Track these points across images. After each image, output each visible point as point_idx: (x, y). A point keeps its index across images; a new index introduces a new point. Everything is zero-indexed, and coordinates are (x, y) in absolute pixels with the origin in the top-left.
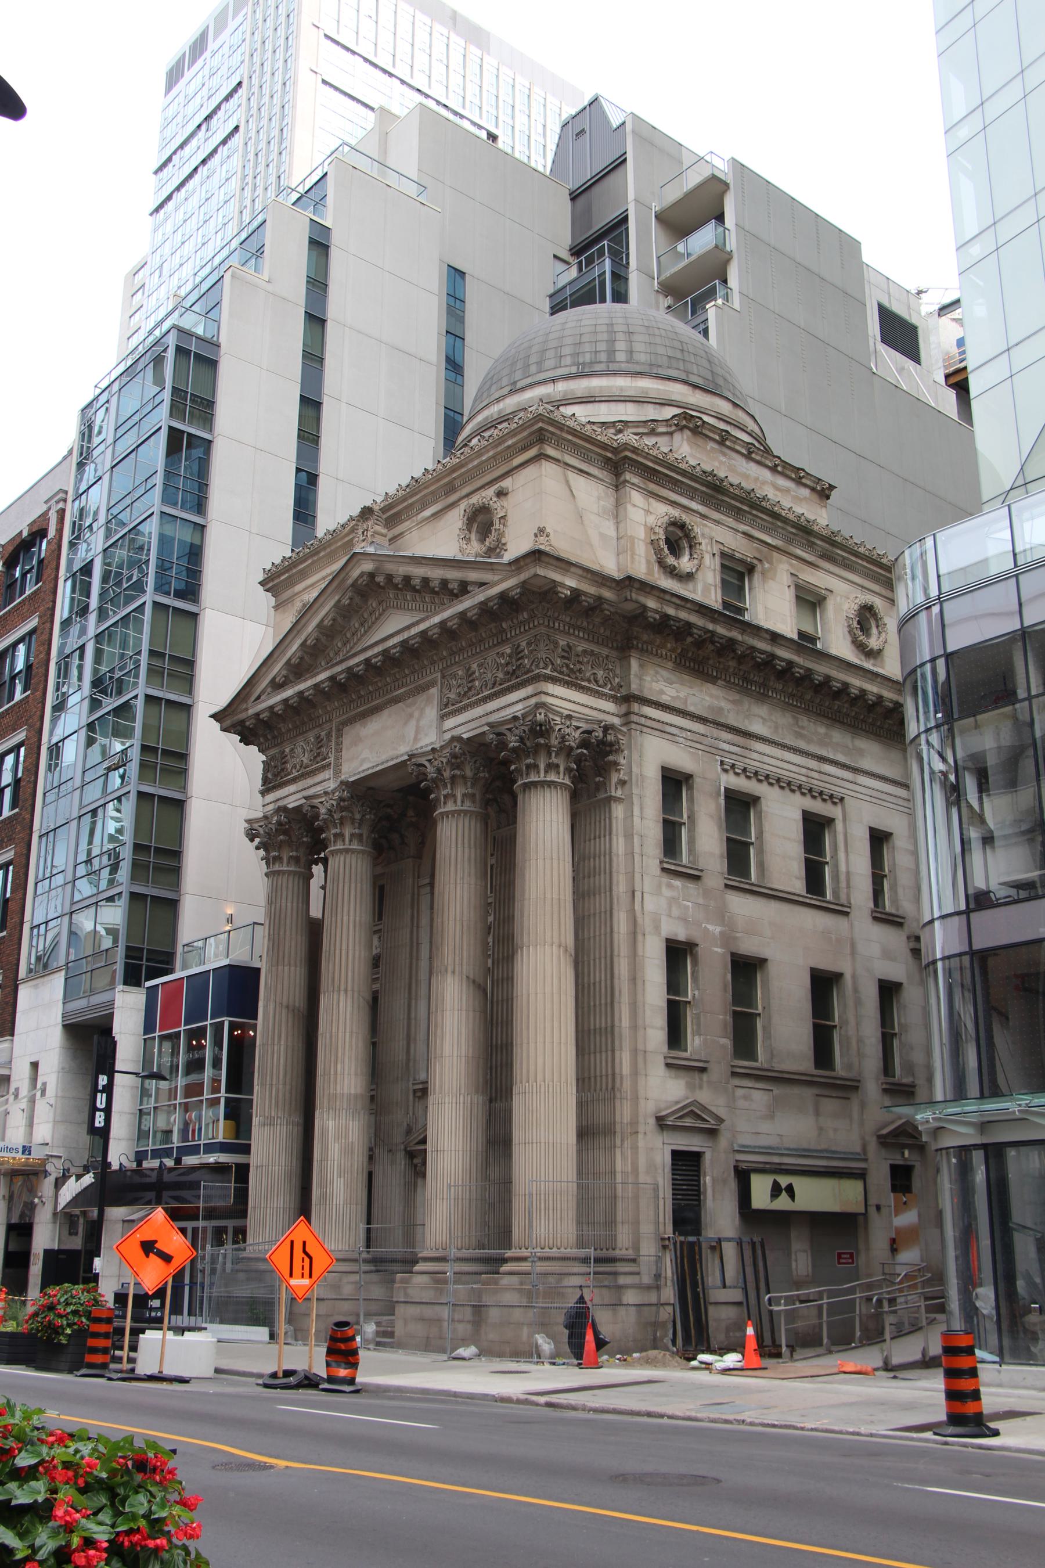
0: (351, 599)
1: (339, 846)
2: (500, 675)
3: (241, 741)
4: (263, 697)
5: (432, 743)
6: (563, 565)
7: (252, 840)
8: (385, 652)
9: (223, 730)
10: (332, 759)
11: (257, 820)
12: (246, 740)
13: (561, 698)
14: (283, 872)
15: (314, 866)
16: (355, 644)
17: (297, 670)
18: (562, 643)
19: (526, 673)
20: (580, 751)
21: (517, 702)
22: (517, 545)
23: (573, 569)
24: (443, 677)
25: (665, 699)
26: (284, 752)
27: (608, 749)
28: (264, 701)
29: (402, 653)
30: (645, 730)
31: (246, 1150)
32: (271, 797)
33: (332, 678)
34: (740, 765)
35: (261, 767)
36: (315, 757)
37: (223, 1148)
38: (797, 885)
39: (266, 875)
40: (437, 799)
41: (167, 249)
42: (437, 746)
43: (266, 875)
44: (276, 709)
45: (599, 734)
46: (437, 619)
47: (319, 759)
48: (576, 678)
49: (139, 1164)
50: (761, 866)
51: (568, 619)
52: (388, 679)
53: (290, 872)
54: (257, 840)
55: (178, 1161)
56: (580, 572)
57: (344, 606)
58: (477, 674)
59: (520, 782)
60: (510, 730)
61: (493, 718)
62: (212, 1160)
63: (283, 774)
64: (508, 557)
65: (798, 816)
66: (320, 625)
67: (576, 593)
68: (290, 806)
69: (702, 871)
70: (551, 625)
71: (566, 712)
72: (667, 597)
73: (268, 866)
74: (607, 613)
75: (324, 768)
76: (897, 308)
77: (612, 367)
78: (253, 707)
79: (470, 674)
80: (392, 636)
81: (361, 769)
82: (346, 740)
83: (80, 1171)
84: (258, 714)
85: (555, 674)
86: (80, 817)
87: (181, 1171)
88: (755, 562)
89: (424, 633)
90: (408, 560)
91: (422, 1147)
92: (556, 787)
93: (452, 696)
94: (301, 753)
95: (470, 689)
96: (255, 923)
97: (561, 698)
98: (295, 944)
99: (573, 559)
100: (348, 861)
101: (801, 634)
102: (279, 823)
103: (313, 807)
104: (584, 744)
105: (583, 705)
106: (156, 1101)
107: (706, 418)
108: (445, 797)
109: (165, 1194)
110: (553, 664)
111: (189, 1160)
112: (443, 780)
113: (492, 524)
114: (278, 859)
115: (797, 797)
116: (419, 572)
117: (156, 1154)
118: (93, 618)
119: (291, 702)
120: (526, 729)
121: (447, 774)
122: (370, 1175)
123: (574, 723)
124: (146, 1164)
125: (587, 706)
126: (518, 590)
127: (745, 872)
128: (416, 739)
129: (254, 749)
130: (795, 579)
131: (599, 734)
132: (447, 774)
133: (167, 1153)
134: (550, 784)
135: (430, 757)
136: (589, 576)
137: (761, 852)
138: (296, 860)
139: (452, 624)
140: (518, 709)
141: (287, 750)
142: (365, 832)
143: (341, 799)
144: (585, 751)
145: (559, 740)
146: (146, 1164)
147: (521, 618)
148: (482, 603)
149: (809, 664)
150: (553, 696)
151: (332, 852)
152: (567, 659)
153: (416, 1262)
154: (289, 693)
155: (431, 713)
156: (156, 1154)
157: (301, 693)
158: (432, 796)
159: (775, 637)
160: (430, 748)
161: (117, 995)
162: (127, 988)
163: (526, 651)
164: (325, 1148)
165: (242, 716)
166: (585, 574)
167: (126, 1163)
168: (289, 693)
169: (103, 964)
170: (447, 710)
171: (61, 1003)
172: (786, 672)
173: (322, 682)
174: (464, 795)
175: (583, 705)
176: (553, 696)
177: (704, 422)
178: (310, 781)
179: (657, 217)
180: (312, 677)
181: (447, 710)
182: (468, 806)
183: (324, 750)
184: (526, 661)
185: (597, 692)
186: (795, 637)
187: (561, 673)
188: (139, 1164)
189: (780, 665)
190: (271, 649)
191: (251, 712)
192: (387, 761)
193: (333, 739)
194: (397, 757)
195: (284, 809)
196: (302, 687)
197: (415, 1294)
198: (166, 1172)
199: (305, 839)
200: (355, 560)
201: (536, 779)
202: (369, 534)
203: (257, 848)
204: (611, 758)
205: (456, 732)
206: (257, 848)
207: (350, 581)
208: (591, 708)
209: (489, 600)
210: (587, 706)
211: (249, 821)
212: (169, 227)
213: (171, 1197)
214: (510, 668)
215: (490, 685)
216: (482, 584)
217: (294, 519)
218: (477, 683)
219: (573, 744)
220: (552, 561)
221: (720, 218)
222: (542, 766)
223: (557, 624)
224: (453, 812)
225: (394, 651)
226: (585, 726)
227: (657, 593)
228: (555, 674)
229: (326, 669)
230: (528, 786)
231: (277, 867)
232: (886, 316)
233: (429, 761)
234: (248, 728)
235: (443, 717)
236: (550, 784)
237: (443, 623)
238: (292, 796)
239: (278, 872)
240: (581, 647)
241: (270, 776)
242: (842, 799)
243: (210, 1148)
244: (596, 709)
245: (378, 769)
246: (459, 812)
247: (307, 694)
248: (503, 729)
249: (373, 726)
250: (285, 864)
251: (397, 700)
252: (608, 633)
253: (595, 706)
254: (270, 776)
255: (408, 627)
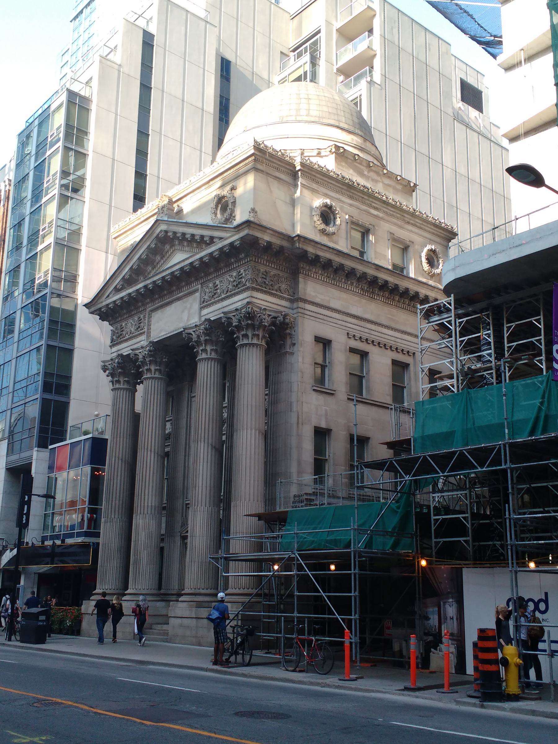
0: (155, 244)
1: (149, 375)
2: (230, 287)
3: (100, 319)
4: (110, 296)
5: (196, 322)
6: (264, 229)
7: (105, 372)
8: (172, 273)
9: (92, 313)
10: (146, 330)
11: (108, 361)
12: (102, 319)
13: (262, 300)
14: (121, 389)
15: (137, 385)
16: (159, 268)
17: (128, 282)
18: (262, 270)
19: (243, 286)
20: (270, 327)
21: (238, 301)
22: (240, 217)
23: (268, 231)
24: (202, 287)
25: (317, 300)
26: (122, 325)
27: (286, 326)
28: (111, 298)
29: (181, 274)
30: (306, 316)
31: (97, 535)
32: (115, 349)
33: (145, 287)
34: (358, 336)
35: (110, 333)
36: (137, 329)
37: (86, 534)
38: (388, 399)
39: (112, 390)
40: (197, 352)
41: (80, 42)
42: (198, 323)
43: (112, 390)
44: (117, 302)
45: (281, 318)
46: (198, 256)
47: (139, 329)
48: (270, 289)
49: (43, 542)
50: (368, 388)
51: (266, 258)
52: (174, 288)
53: (124, 389)
54: (108, 372)
55: (63, 541)
56: (271, 232)
57: (152, 248)
58: (219, 286)
59: (239, 344)
60: (234, 316)
61: (226, 310)
62: (80, 541)
63: (121, 337)
64: (235, 223)
65: (390, 362)
66: (139, 258)
67: (269, 244)
68: (125, 354)
69: (335, 391)
70: (257, 260)
71: (263, 307)
72: (319, 246)
73: (113, 386)
74: (287, 255)
75: (141, 334)
76: (471, 81)
77: (299, 118)
78: (105, 301)
79: (215, 286)
80: (175, 265)
81: (160, 336)
82: (153, 320)
83: (12, 546)
84: (108, 305)
85: (258, 287)
86: (17, 357)
87: (64, 547)
88: (370, 226)
89: (191, 264)
90: (184, 225)
91: (187, 534)
92: (253, 346)
93: (206, 297)
94: (130, 325)
95: (215, 294)
96: (107, 415)
97: (262, 300)
98: (125, 426)
99: (269, 226)
100: (153, 383)
101: (394, 266)
102: (118, 363)
103: (136, 355)
104: (273, 324)
105: (273, 303)
106: (53, 509)
107: (347, 148)
108: (201, 350)
109: (56, 559)
110: (257, 281)
111: (69, 541)
112: (200, 342)
113: (228, 206)
114: (118, 382)
115: (389, 352)
116: (189, 231)
117: (52, 538)
118: (24, 250)
119: (125, 299)
120: (242, 315)
121: (202, 339)
122: (162, 549)
123: (268, 313)
124: (46, 543)
125: (275, 304)
126: (239, 242)
127: (360, 392)
128: (188, 320)
129: (106, 323)
130: (392, 235)
131: (281, 318)
132: (202, 339)
133: (57, 537)
134: (253, 345)
135: (194, 330)
136: (277, 234)
137: (368, 381)
138: (128, 382)
139: (206, 259)
140: (239, 305)
141: (123, 324)
142: (162, 369)
143: (150, 351)
144: (273, 328)
145: (259, 321)
146: (46, 543)
147: (241, 256)
148: (220, 248)
149: (397, 282)
150: (256, 298)
151: (145, 379)
152: (265, 279)
153: (181, 595)
154: (123, 294)
155: (196, 306)
156: (52, 538)
157: (130, 294)
158: (195, 350)
159: (378, 268)
160: (194, 324)
161: (34, 452)
162: (40, 449)
163: (243, 275)
164: (137, 534)
165: (100, 306)
166: (274, 233)
167: (35, 542)
168: (123, 294)
169: (27, 436)
170: (204, 305)
171: (5, 458)
172: (385, 286)
173: (140, 288)
174: (156, 370)
175: (273, 303)
176: (256, 298)
177: (345, 150)
178: (135, 341)
179: (337, 30)
180: (135, 286)
181: (204, 305)
182: (214, 355)
183: (142, 324)
184: (243, 279)
185: (281, 296)
186: (390, 267)
187: (261, 286)
188: (43, 542)
189: (380, 282)
190: (116, 268)
191: (104, 304)
192: (173, 331)
193: (147, 319)
194: (178, 329)
195: (121, 356)
196: (130, 290)
197: (179, 613)
198: (56, 547)
199: (132, 372)
200: (158, 223)
201: (247, 342)
202: (165, 209)
203: (108, 376)
204: (288, 331)
205: (207, 317)
206: (108, 376)
207: (155, 235)
208: (278, 305)
209: (224, 246)
210: (275, 304)
211: (103, 362)
212: (82, 29)
213: (58, 560)
214: (235, 283)
215: (225, 292)
216: (221, 238)
217: (134, 199)
218: (219, 291)
219: (266, 324)
220: (256, 227)
221: (371, 31)
222: (250, 335)
223: (259, 260)
224: (205, 359)
225: (177, 273)
226: (274, 314)
227: (313, 244)
228: (258, 287)
229: (142, 282)
230: (242, 346)
231: (117, 386)
232: (464, 86)
233: (194, 331)
234: (103, 312)
235: (201, 308)
236: (253, 345)
237: (201, 259)
238: (125, 349)
239: (118, 389)
240: (273, 272)
241: (114, 337)
242: (414, 354)
243: (79, 535)
244: (280, 305)
245: (169, 335)
246: (208, 359)
247: (133, 295)
248: (231, 315)
249: (170, 310)
250: (122, 385)
251: (179, 299)
252: (287, 265)
253: (279, 304)
254: (114, 337)
255: (183, 261)
